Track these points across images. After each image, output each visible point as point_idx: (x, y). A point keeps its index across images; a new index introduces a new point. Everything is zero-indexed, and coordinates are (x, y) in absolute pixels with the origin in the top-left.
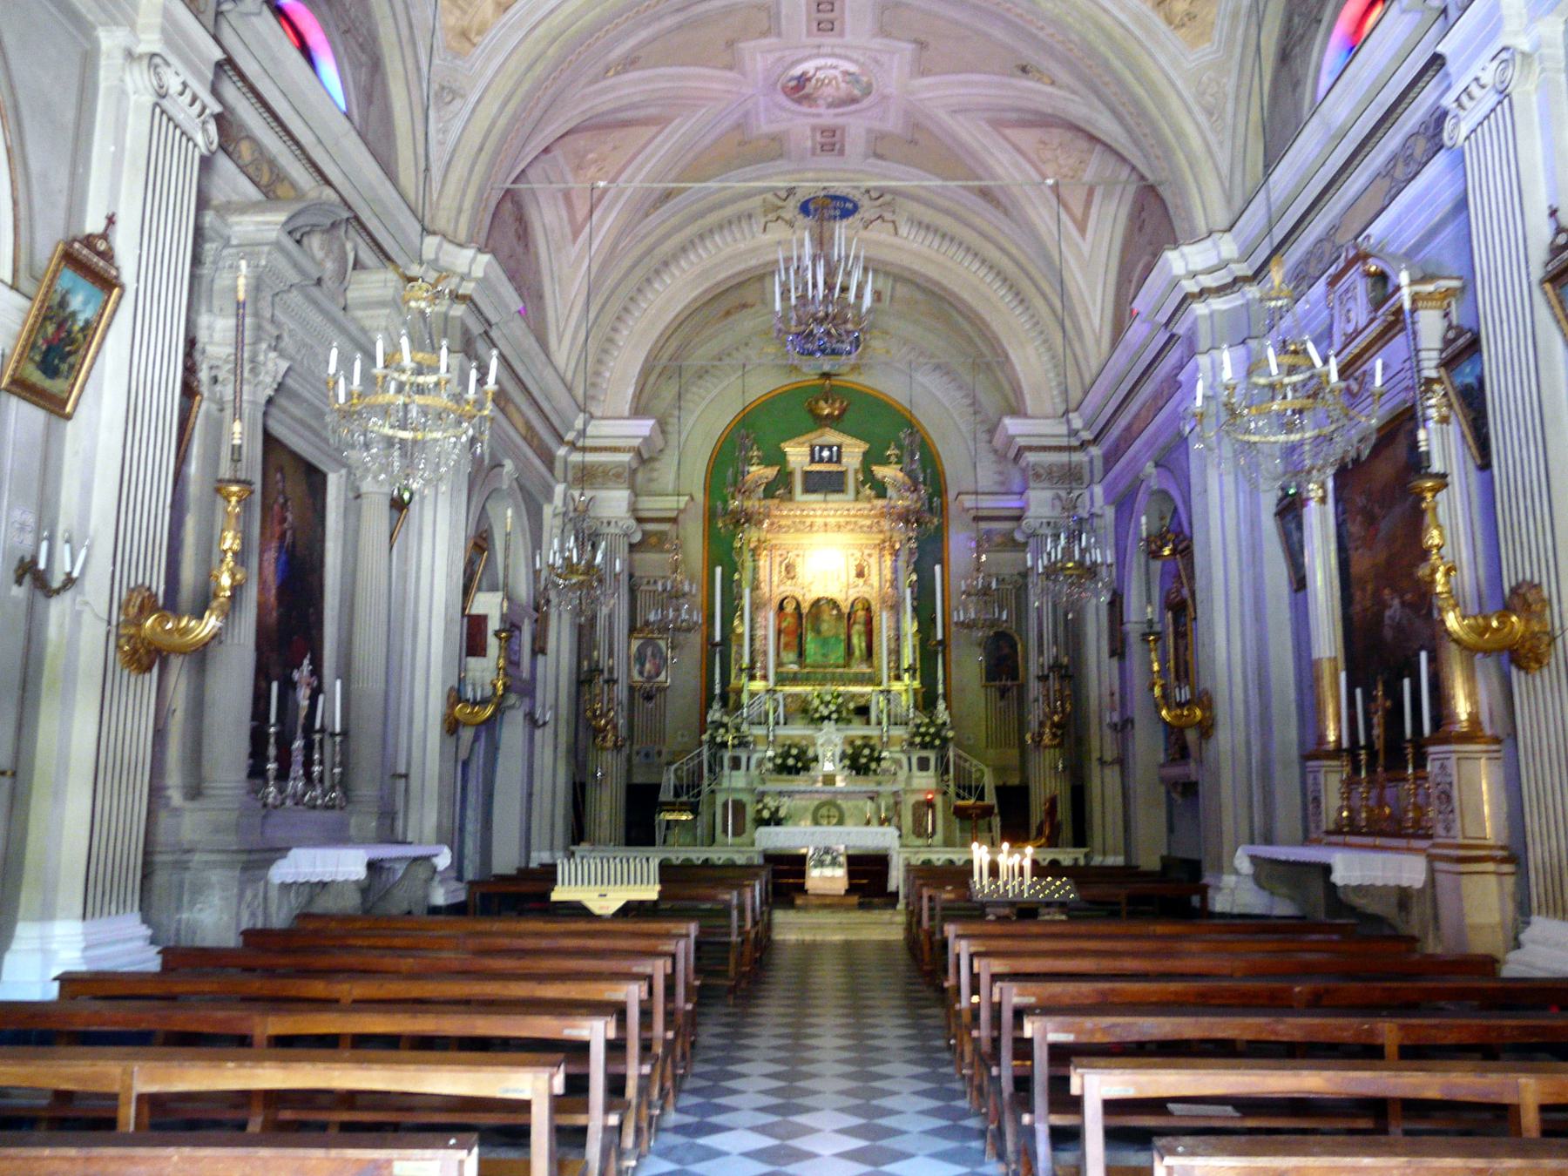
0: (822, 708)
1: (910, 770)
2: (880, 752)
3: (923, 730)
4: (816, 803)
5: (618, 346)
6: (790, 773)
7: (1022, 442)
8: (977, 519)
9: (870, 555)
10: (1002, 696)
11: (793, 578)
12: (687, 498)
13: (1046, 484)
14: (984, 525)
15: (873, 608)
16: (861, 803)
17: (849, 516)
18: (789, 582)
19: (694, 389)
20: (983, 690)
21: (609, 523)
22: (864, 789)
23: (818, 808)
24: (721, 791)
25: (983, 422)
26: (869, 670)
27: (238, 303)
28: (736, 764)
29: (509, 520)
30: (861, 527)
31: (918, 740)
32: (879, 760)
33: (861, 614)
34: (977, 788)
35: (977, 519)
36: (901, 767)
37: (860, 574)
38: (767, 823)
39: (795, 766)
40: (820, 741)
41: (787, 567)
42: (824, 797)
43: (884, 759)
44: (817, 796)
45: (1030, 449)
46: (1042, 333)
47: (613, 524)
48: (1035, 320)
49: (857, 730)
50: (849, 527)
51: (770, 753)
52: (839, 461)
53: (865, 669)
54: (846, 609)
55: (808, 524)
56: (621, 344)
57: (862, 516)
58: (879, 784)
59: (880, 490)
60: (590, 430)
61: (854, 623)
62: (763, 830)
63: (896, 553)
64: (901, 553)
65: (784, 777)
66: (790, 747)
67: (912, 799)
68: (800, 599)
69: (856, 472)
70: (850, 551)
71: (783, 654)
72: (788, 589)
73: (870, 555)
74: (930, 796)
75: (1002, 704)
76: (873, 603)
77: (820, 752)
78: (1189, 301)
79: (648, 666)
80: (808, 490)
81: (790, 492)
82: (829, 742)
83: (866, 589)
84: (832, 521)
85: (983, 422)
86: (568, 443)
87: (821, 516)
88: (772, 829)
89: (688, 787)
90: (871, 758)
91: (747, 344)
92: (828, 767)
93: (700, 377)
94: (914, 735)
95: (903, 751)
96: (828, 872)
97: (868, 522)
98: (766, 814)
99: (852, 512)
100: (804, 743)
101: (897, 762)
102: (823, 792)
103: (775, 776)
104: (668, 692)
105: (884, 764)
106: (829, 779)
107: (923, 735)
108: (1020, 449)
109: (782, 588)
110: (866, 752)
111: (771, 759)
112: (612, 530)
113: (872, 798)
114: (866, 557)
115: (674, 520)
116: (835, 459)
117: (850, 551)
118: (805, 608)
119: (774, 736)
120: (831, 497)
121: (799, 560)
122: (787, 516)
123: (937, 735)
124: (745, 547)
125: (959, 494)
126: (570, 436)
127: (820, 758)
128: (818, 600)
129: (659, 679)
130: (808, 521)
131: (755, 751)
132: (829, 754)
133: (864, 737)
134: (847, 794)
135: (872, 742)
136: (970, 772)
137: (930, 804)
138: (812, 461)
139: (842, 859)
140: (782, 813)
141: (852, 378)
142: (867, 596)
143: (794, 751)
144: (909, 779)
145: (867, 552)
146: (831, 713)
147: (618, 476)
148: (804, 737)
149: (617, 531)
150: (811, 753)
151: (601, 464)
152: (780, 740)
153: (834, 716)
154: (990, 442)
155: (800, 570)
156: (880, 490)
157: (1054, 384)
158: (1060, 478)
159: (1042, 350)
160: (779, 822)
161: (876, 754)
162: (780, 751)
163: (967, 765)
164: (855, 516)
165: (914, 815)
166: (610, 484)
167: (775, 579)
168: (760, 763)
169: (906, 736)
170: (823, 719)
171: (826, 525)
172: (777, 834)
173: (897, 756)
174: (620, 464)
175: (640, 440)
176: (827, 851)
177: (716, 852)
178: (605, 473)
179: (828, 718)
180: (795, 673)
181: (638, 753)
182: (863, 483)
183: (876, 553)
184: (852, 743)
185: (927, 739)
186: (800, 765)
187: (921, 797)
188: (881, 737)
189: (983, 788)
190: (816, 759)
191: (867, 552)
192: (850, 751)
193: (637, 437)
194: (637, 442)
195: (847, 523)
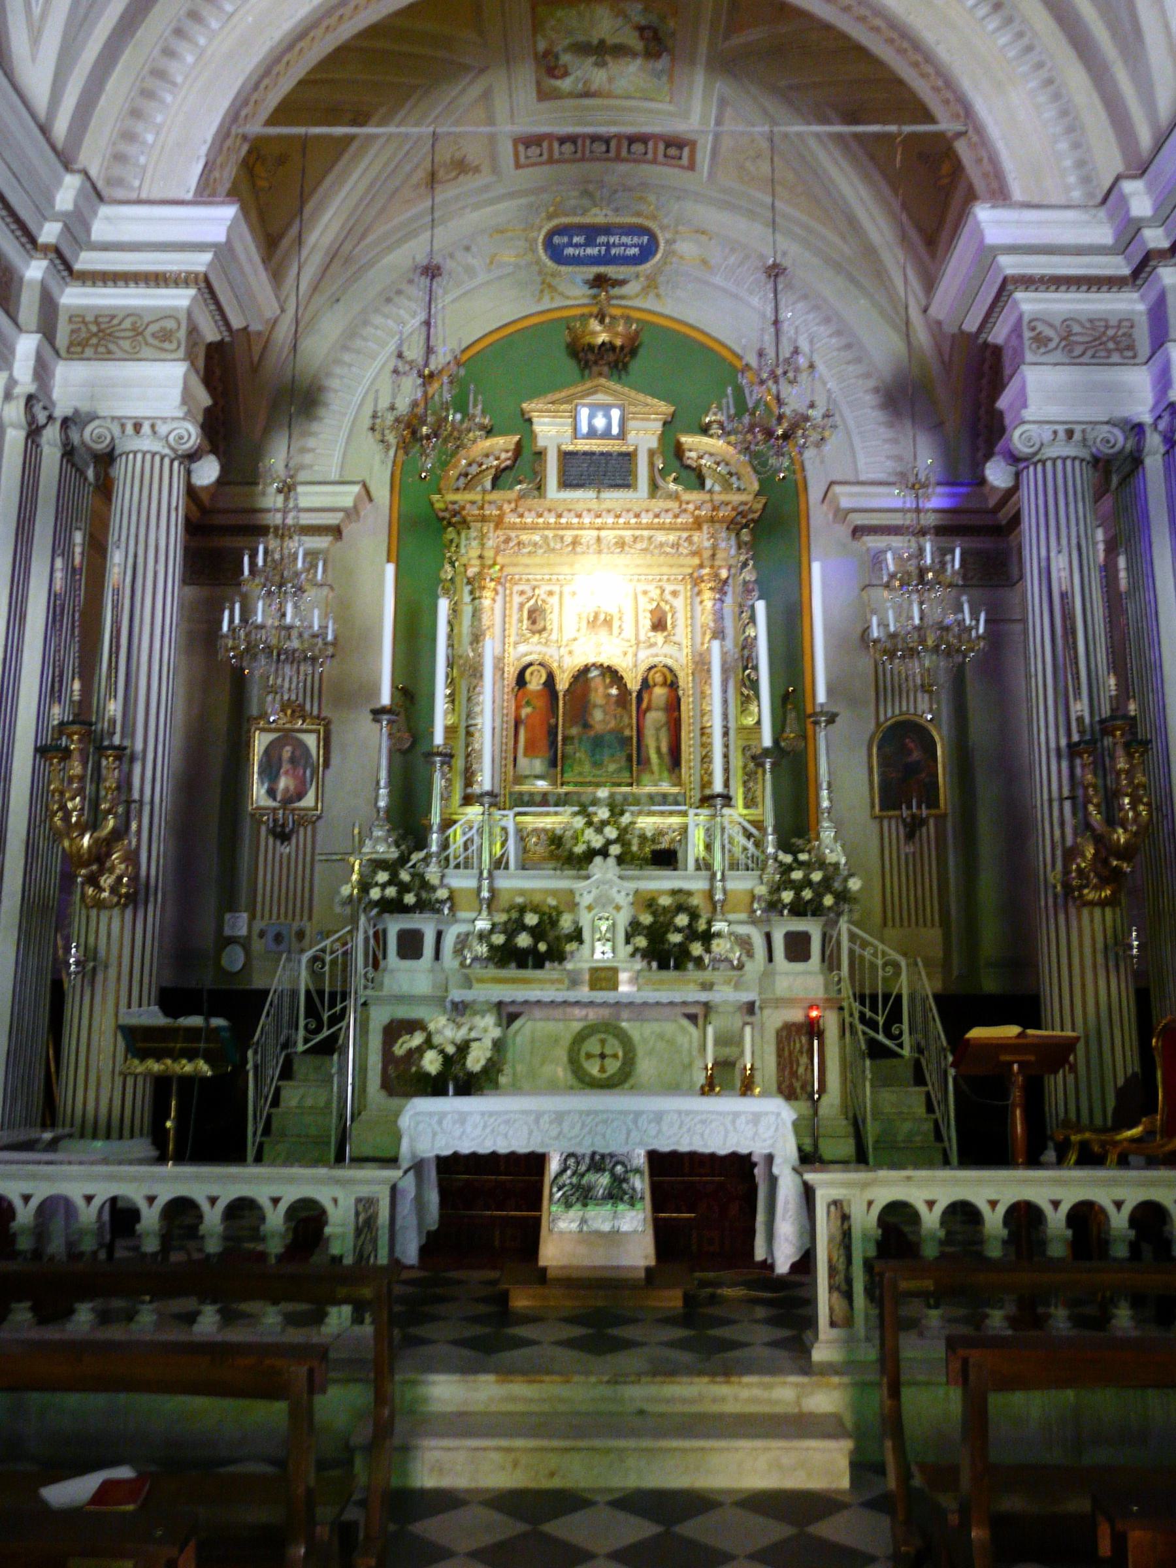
0: (590, 834)
1: (771, 959)
2: (709, 923)
3: (797, 875)
4: (577, 1026)
5: (174, 84)
6: (522, 965)
7: (1010, 265)
8: (858, 532)
9: (675, 594)
10: (910, 836)
11: (540, 632)
12: (356, 489)
13: (1058, 356)
14: (873, 542)
15: (681, 683)
16: (669, 1028)
17: (639, 527)
18: (536, 638)
19: (378, 320)
20: (874, 827)
21: (137, 427)
22: (678, 997)
23: (580, 1038)
24: (380, 1000)
25: (868, 375)
26: (675, 790)
27: (74, 569)
28: (410, 945)
29: (78, 550)
30: (661, 545)
31: (787, 896)
32: (707, 938)
33: (659, 692)
34: (886, 997)
35: (858, 532)
36: (750, 954)
37: (659, 625)
38: (435, 1087)
39: (533, 950)
40: (586, 900)
41: (531, 612)
42: (593, 1015)
43: (719, 935)
44: (577, 1012)
45: (1029, 282)
46: (1040, 65)
47: (146, 428)
48: (1025, 41)
49: (660, 883)
50: (639, 546)
51: (482, 924)
52: (622, 435)
53: (666, 787)
54: (633, 685)
55: (568, 540)
56: (179, 79)
57: (662, 528)
58: (707, 986)
59: (696, 478)
60: (100, 230)
61: (648, 709)
62: (423, 1105)
63: (721, 587)
64: (729, 589)
65: (512, 972)
66: (522, 910)
67: (774, 1019)
68: (555, 665)
69: (652, 453)
70: (641, 587)
71: (523, 761)
72: (529, 649)
73: (675, 594)
74: (814, 1014)
75: (910, 849)
76: (681, 675)
77: (585, 919)
78: (1152, 263)
79: (283, 783)
80: (565, 483)
81: (539, 488)
82: (603, 901)
83: (670, 649)
84: (609, 535)
85: (868, 375)
86: (46, 249)
87: (592, 527)
88: (450, 1104)
89: (333, 995)
90: (692, 934)
91: (467, 249)
92: (601, 953)
93: (389, 300)
94: (776, 889)
95: (754, 922)
96: (601, 1218)
97: (672, 537)
98: (431, 1063)
99: (645, 519)
100: (552, 902)
101: (745, 944)
102: (591, 1004)
103: (493, 971)
104: (321, 825)
105: (720, 947)
106: (604, 978)
107: (798, 887)
108: (1005, 280)
109: (522, 648)
110: (682, 920)
111: (482, 936)
112: (146, 443)
113: (692, 1018)
114: (668, 596)
115: (336, 531)
116: (615, 430)
117: (641, 587)
118: (562, 685)
119: (492, 890)
120: (609, 494)
121: (554, 600)
122: (534, 528)
123: (826, 885)
124: (458, 579)
125: (832, 483)
126: (49, 233)
127: (586, 935)
128: (586, 670)
129: (303, 803)
130: (569, 535)
131: (453, 918)
132: (604, 926)
133: (674, 893)
134: (638, 1009)
135: (695, 901)
136: (873, 966)
137: (813, 1029)
138: (576, 434)
139: (640, 1184)
140: (476, 1060)
141: (649, 303)
142: (670, 662)
143: (531, 919)
144: (767, 976)
145: (669, 588)
146: (609, 843)
147: (165, 336)
148: (554, 893)
149: (157, 447)
150: (566, 923)
151: (132, 314)
152: (503, 901)
153: (615, 850)
154: (925, 311)
155: (552, 619)
156: (696, 478)
157: (1068, 163)
158: (1087, 346)
159: (1042, 99)
160: (469, 1085)
161: (702, 926)
162: (501, 918)
163: (867, 954)
164: (649, 527)
165: (780, 1054)
166: (147, 352)
167: (513, 631)
168: (462, 943)
169: (762, 890)
170: (591, 854)
171: (599, 539)
172: (462, 1118)
173: (742, 930)
174: (169, 314)
175: (208, 257)
176: (598, 1163)
177: (270, 1180)
178: (137, 332)
179: (604, 852)
180: (545, 795)
181: (262, 934)
182: (664, 473)
183: (684, 589)
184: (650, 904)
185: (807, 894)
186: (542, 947)
187: (796, 1015)
188: (710, 894)
189: (899, 997)
190: (577, 936)
191: (669, 588)
192: (646, 919)
193: (199, 247)
194: (200, 262)
195: (635, 539)
